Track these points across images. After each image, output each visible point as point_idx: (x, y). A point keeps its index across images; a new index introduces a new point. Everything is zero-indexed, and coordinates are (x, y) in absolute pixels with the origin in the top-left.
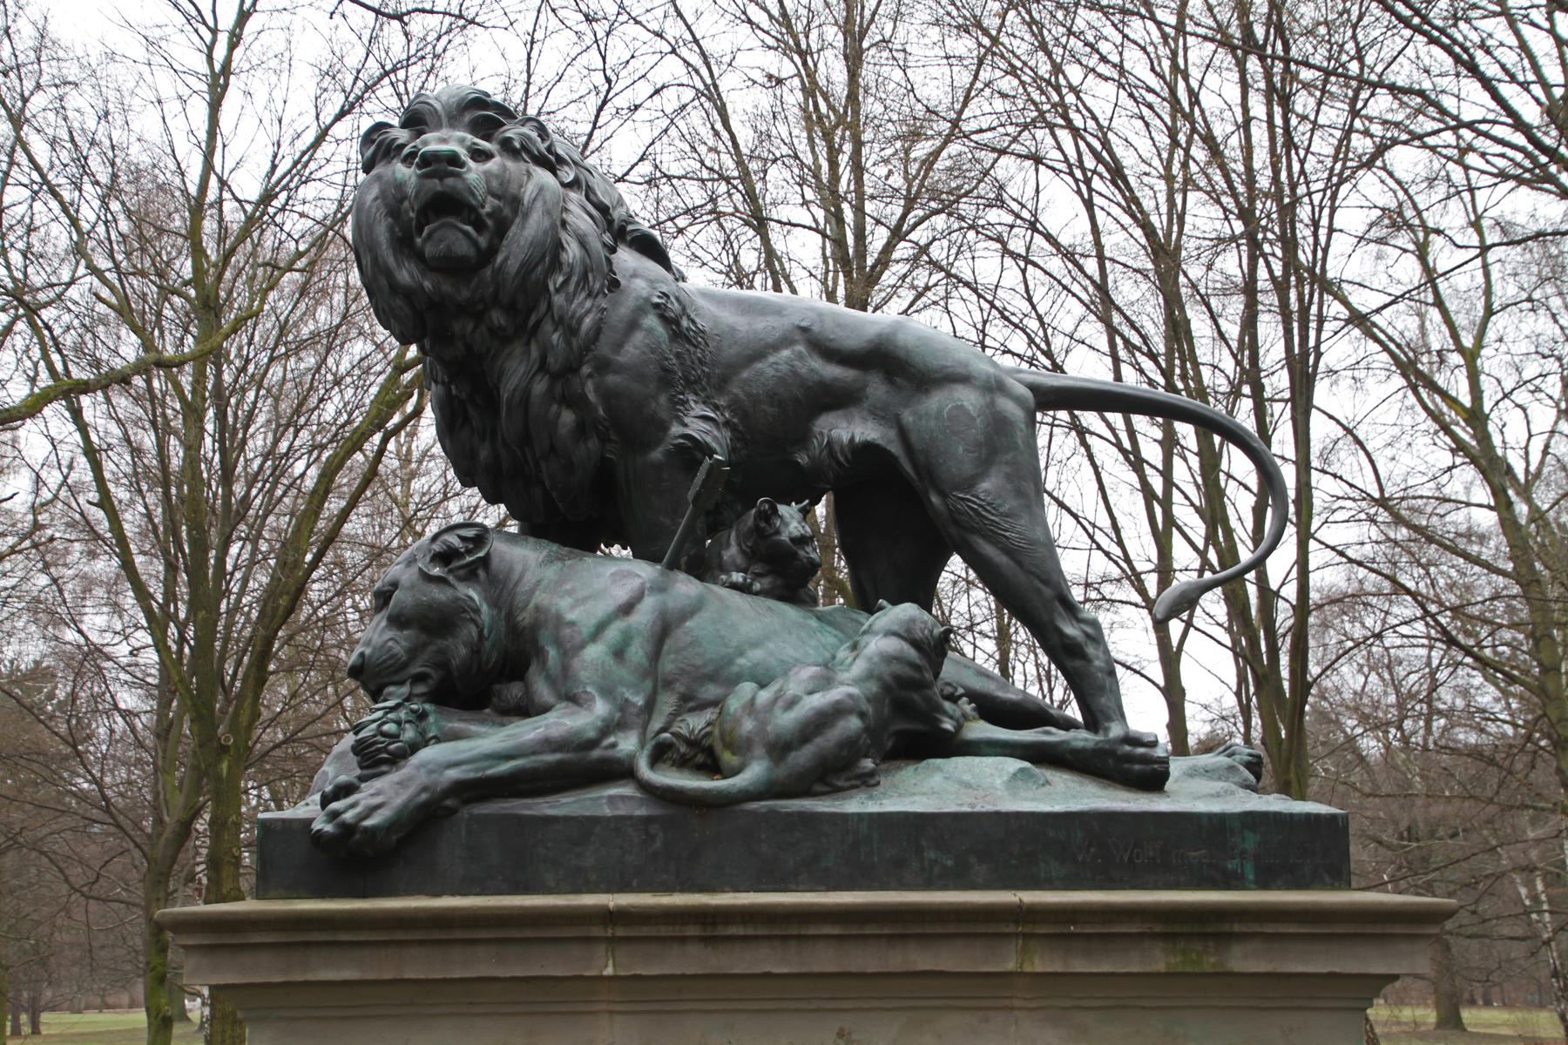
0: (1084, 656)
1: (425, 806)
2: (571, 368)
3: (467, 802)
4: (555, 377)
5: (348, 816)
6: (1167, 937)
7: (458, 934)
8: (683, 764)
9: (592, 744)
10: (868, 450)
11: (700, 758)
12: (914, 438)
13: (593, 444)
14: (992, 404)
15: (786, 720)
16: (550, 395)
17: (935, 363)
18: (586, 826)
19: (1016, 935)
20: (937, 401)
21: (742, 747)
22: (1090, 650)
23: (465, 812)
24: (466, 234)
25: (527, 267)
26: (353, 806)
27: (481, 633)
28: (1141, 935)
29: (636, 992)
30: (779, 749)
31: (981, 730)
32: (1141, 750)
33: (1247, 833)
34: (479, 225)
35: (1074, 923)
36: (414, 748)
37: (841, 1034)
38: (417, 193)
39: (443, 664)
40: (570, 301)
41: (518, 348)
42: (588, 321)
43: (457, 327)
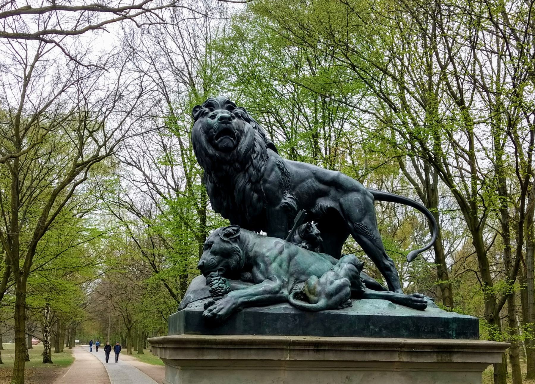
1: (234, 309)
2: (258, 182)
3: (244, 308)
4: (252, 184)
5: (214, 311)
8: (302, 300)
9: (277, 292)
11: (302, 297)
12: (344, 206)
13: (261, 204)
14: (365, 198)
15: (331, 288)
17: (350, 186)
18: (277, 317)
19: (399, 351)
20: (354, 197)
21: (318, 295)
22: (392, 269)
23: (244, 311)
24: (232, 140)
25: (247, 151)
26: (215, 308)
27: (240, 257)
29: (295, 366)
30: (330, 296)
31: (368, 291)
32: (420, 299)
33: (454, 324)
34: (234, 138)
35: (414, 348)
36: (227, 292)
37: (347, 378)
38: (218, 128)
39: (227, 266)
40: (258, 162)
41: (241, 175)
42: (263, 168)
43: (224, 167)
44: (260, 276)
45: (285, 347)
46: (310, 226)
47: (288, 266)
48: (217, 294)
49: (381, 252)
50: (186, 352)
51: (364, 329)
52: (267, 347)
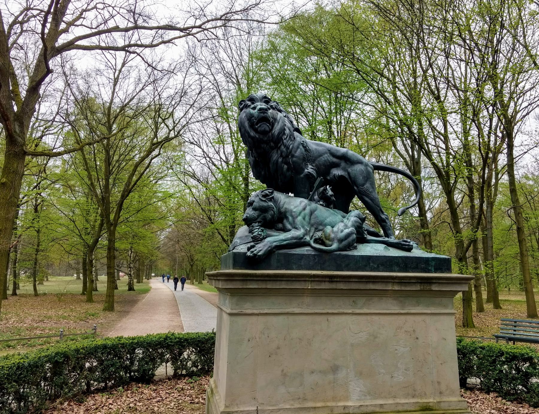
0: (386, 222)
1: (270, 250)
2: (287, 156)
5: (255, 252)
6: (421, 283)
7: (279, 279)
8: (320, 244)
9: (302, 238)
10: (341, 177)
11: (320, 242)
12: (351, 175)
14: (367, 169)
15: (341, 235)
16: (282, 162)
17: (355, 159)
18: (302, 256)
21: (332, 240)
22: (387, 221)
23: (277, 252)
25: (279, 134)
27: (274, 212)
28: (416, 282)
29: (315, 293)
30: (340, 241)
31: (369, 237)
34: (270, 124)
36: (264, 238)
37: (353, 302)
39: (265, 219)
41: (275, 151)
43: (262, 146)
44: (289, 226)
45: (307, 279)
46: (325, 190)
47: (310, 219)
48: (257, 240)
49: (379, 208)
50: (234, 283)
51: (366, 266)
52: (294, 279)
